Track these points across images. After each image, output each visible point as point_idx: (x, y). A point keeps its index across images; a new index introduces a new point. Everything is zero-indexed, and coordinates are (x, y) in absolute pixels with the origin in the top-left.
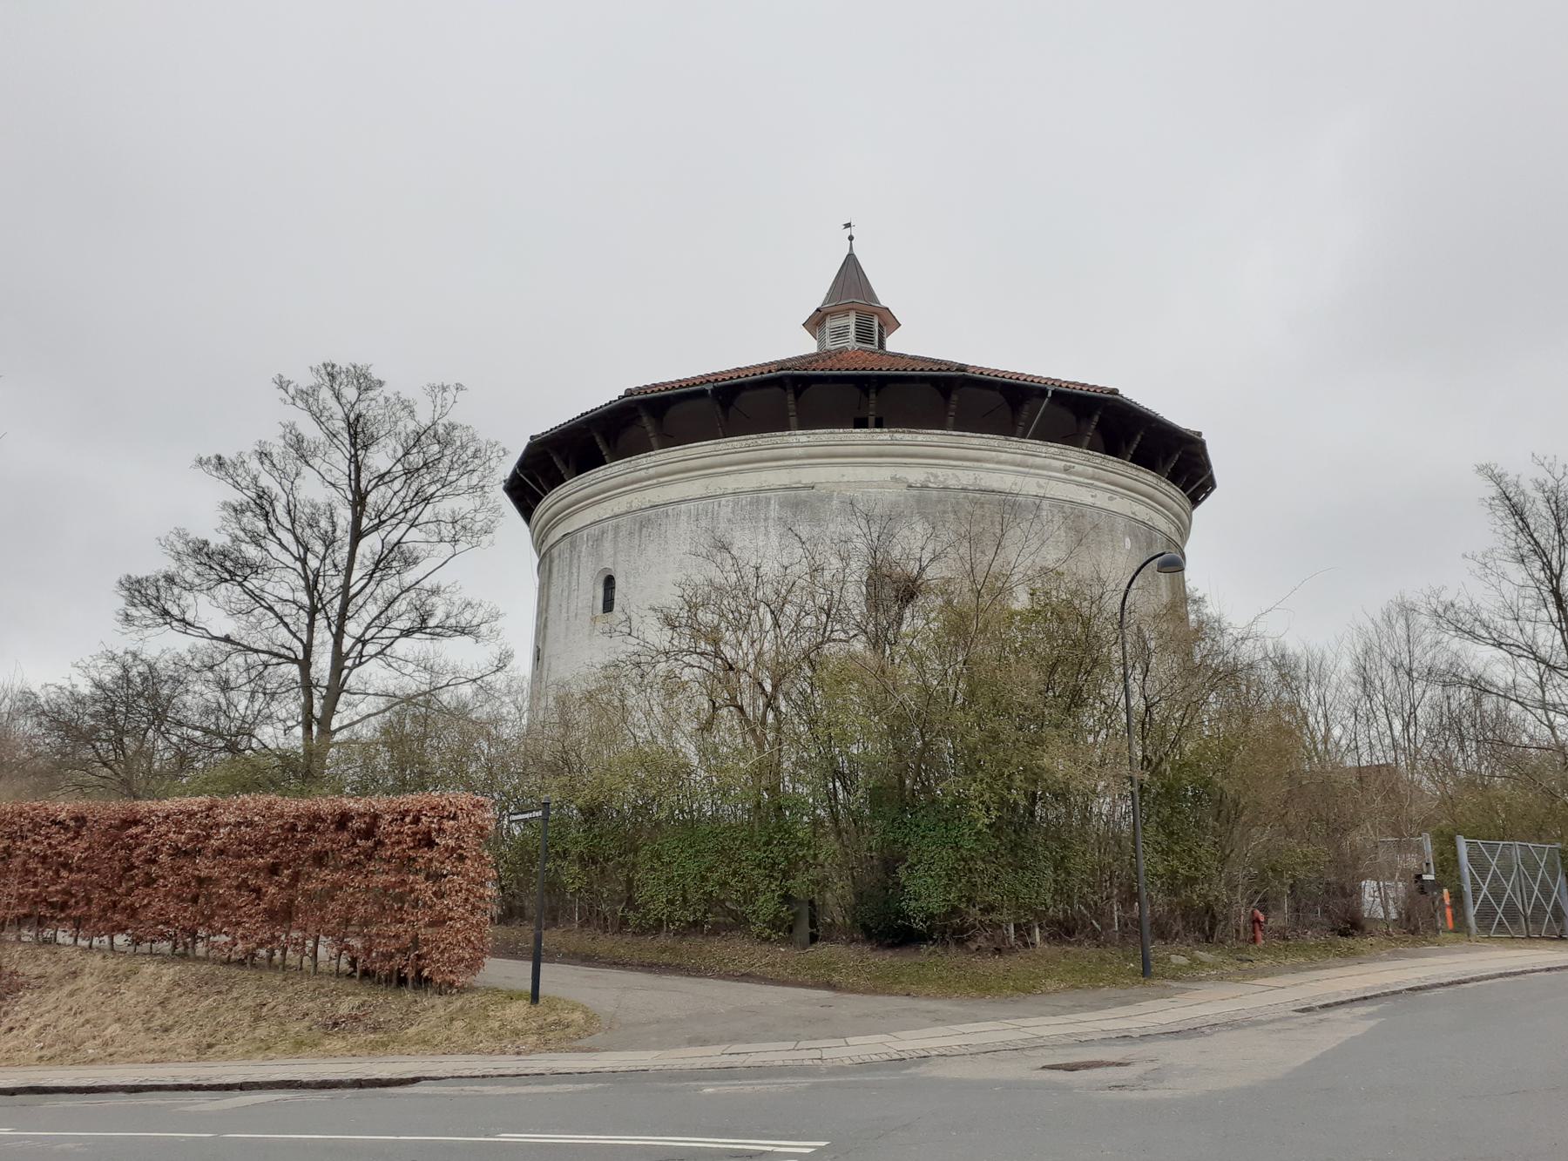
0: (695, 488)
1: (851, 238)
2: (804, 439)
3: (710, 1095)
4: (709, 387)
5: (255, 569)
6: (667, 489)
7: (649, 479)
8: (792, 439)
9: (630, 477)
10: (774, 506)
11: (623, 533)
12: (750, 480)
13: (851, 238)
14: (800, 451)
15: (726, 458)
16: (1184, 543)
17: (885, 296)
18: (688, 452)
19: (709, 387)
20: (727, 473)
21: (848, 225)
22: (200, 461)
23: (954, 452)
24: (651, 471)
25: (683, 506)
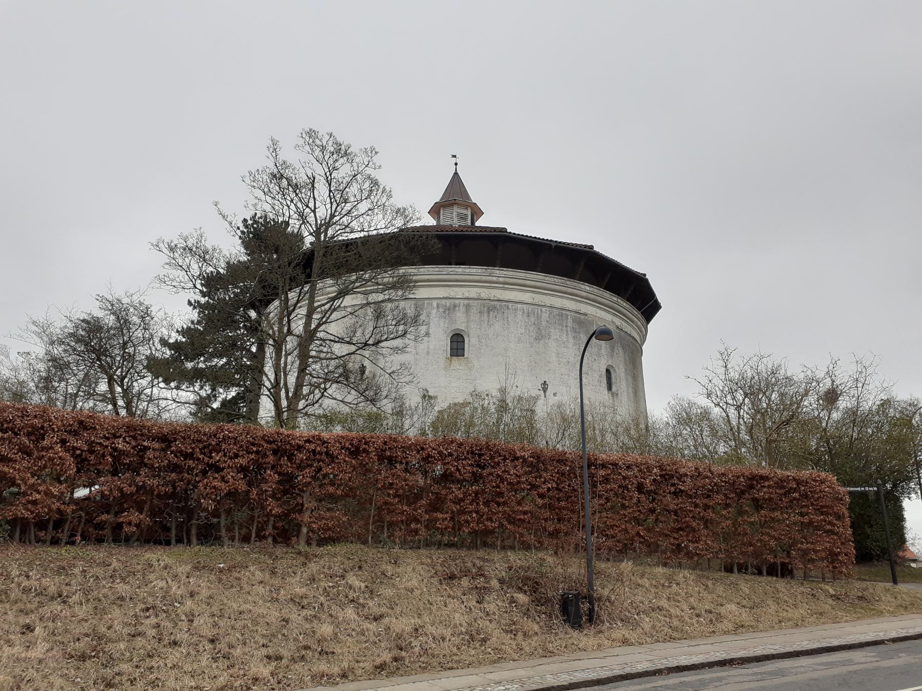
0: (526, 297)
1: (456, 164)
2: (588, 288)
3: (87, 499)
4: (554, 244)
5: (49, 361)
6: (506, 292)
7: (497, 283)
8: (583, 286)
9: (484, 278)
10: (570, 320)
11: (474, 310)
12: (558, 302)
13: (456, 164)
14: (584, 294)
15: (528, 283)
16: (643, 344)
17: (475, 196)
18: (528, 275)
19: (554, 244)
20: (544, 294)
21: (454, 156)
22: (277, 177)
23: (570, 290)
24: (501, 280)
25: (519, 306)
